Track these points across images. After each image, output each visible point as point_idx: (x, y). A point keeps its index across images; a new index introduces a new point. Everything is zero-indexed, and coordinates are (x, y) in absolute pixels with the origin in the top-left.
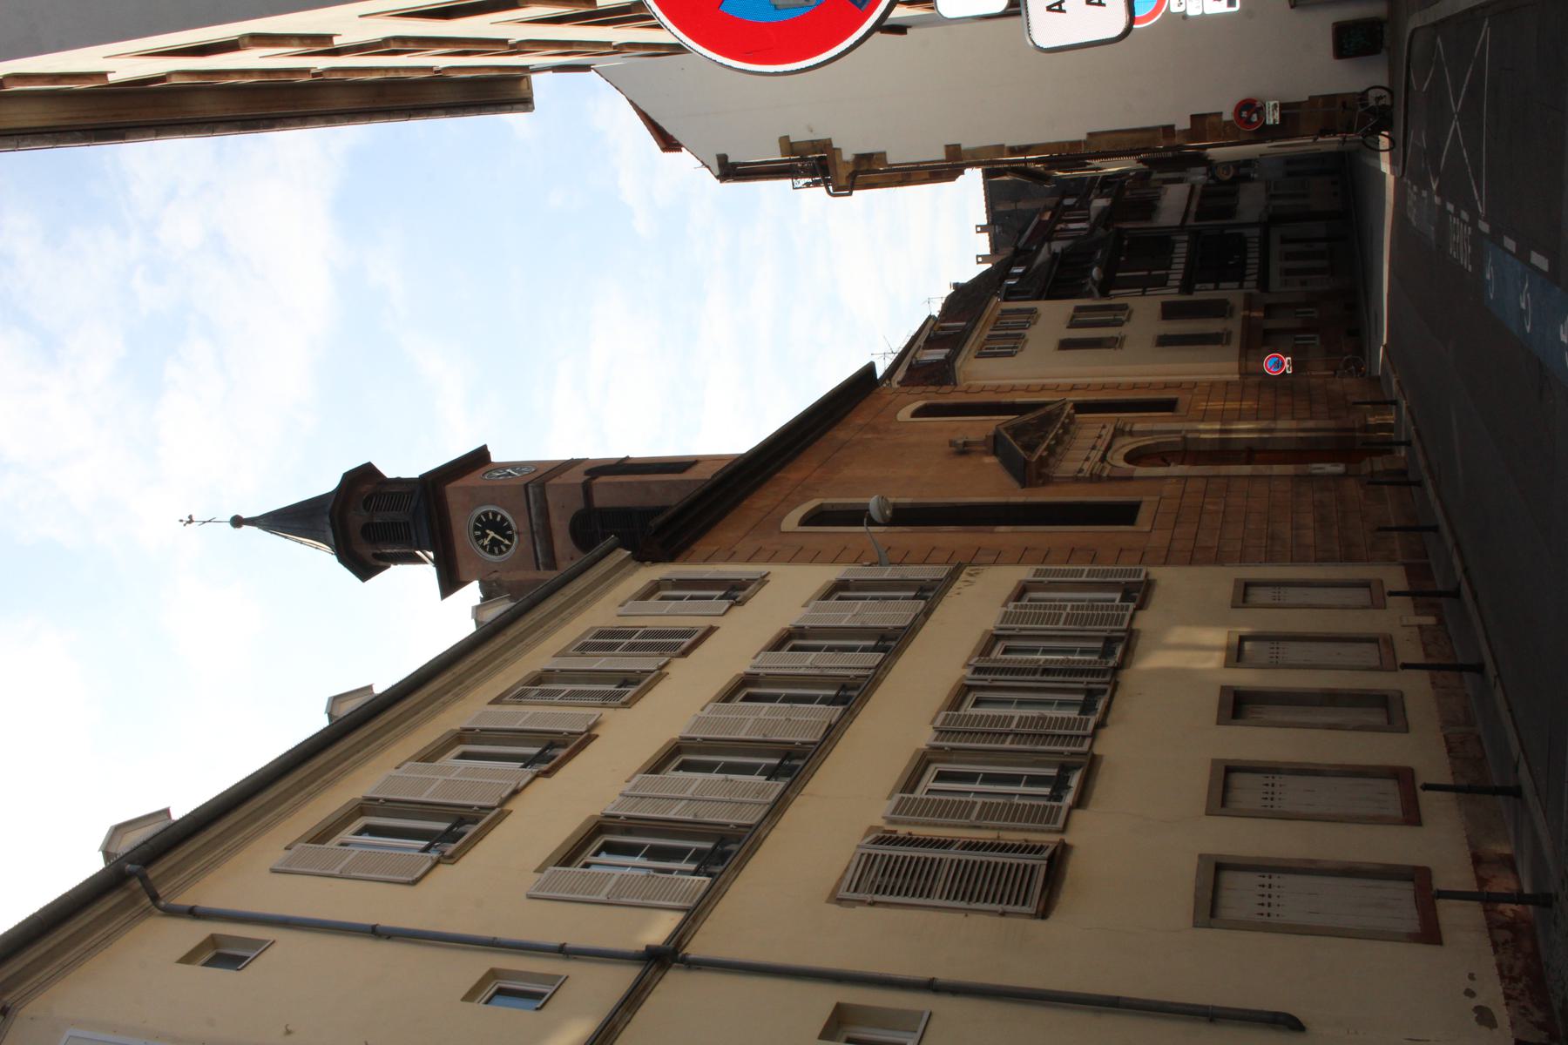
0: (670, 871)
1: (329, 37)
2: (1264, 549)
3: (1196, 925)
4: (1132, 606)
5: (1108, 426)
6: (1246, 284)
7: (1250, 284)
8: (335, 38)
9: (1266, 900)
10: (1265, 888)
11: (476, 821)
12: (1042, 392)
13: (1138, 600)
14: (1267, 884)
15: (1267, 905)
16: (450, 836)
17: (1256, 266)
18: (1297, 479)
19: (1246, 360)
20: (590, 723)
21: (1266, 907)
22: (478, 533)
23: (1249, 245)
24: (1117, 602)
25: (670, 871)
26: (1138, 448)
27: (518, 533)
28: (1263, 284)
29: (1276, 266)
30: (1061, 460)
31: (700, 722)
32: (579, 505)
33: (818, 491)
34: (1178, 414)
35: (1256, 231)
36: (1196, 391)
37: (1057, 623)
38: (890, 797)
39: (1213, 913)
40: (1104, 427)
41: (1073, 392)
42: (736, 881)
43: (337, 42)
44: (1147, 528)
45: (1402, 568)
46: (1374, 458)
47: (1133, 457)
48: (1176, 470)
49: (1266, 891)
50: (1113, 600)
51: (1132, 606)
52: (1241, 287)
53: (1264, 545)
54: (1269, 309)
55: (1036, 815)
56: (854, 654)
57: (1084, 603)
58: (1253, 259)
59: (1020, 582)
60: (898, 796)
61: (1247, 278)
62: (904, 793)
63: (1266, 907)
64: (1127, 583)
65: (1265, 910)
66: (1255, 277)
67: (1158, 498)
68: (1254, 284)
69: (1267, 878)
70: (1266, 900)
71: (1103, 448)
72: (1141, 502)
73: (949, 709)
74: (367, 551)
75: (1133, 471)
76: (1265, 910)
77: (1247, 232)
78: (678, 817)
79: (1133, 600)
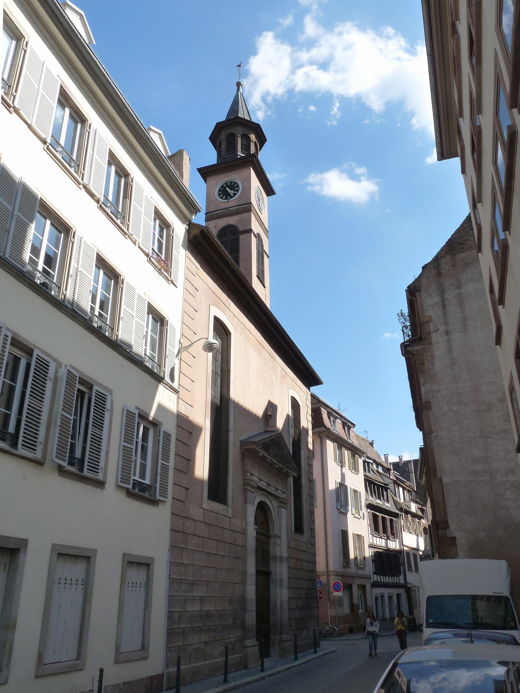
0: (146, 345)
1: (480, 202)
2: (184, 578)
3: (54, 545)
4: (130, 487)
5: (285, 495)
6: (375, 576)
7: (375, 578)
8: (480, 204)
9: (68, 581)
10: (76, 582)
11: (122, 223)
12: (307, 465)
13: (133, 491)
14: (66, 582)
15: (66, 582)
16: (159, 260)
17: (385, 581)
18: (243, 600)
19: (335, 575)
20: (21, 112)
21: (132, 585)
22: (229, 184)
23: (395, 578)
24: (133, 477)
25: (146, 345)
26: (270, 510)
27: (228, 202)
28: (375, 585)
29: (386, 591)
30: (259, 465)
31: (132, 289)
32: (241, 229)
33: (241, 334)
34: (293, 533)
35: (402, 581)
36: (309, 545)
37: (162, 459)
38: (137, 408)
39: (130, 563)
40: (284, 493)
41: (307, 480)
42: (79, 326)
43: (479, 205)
44: (205, 506)
45: (159, 672)
46: (258, 647)
47: (262, 507)
48: (252, 531)
49: (138, 585)
50: (134, 475)
51: (130, 487)
52: (374, 573)
53: (187, 578)
54: (363, 587)
55: (163, 488)
56: (90, 301)
57: (134, 456)
58: (388, 580)
59: (162, 424)
60: (137, 412)
61: (378, 576)
62: (79, 379)
63: (132, 585)
64: (156, 487)
65: (131, 585)
66: (379, 580)
67: (230, 515)
68: (376, 580)
69: (144, 586)
70: (134, 585)
71: (268, 490)
72: (228, 506)
73: (13, 338)
74: (223, 136)
75: (253, 504)
76: (131, 585)
77: (402, 577)
78: (167, 348)
79: (134, 488)
